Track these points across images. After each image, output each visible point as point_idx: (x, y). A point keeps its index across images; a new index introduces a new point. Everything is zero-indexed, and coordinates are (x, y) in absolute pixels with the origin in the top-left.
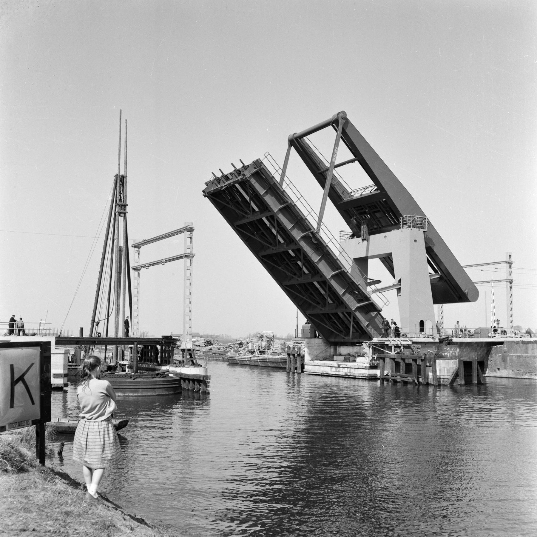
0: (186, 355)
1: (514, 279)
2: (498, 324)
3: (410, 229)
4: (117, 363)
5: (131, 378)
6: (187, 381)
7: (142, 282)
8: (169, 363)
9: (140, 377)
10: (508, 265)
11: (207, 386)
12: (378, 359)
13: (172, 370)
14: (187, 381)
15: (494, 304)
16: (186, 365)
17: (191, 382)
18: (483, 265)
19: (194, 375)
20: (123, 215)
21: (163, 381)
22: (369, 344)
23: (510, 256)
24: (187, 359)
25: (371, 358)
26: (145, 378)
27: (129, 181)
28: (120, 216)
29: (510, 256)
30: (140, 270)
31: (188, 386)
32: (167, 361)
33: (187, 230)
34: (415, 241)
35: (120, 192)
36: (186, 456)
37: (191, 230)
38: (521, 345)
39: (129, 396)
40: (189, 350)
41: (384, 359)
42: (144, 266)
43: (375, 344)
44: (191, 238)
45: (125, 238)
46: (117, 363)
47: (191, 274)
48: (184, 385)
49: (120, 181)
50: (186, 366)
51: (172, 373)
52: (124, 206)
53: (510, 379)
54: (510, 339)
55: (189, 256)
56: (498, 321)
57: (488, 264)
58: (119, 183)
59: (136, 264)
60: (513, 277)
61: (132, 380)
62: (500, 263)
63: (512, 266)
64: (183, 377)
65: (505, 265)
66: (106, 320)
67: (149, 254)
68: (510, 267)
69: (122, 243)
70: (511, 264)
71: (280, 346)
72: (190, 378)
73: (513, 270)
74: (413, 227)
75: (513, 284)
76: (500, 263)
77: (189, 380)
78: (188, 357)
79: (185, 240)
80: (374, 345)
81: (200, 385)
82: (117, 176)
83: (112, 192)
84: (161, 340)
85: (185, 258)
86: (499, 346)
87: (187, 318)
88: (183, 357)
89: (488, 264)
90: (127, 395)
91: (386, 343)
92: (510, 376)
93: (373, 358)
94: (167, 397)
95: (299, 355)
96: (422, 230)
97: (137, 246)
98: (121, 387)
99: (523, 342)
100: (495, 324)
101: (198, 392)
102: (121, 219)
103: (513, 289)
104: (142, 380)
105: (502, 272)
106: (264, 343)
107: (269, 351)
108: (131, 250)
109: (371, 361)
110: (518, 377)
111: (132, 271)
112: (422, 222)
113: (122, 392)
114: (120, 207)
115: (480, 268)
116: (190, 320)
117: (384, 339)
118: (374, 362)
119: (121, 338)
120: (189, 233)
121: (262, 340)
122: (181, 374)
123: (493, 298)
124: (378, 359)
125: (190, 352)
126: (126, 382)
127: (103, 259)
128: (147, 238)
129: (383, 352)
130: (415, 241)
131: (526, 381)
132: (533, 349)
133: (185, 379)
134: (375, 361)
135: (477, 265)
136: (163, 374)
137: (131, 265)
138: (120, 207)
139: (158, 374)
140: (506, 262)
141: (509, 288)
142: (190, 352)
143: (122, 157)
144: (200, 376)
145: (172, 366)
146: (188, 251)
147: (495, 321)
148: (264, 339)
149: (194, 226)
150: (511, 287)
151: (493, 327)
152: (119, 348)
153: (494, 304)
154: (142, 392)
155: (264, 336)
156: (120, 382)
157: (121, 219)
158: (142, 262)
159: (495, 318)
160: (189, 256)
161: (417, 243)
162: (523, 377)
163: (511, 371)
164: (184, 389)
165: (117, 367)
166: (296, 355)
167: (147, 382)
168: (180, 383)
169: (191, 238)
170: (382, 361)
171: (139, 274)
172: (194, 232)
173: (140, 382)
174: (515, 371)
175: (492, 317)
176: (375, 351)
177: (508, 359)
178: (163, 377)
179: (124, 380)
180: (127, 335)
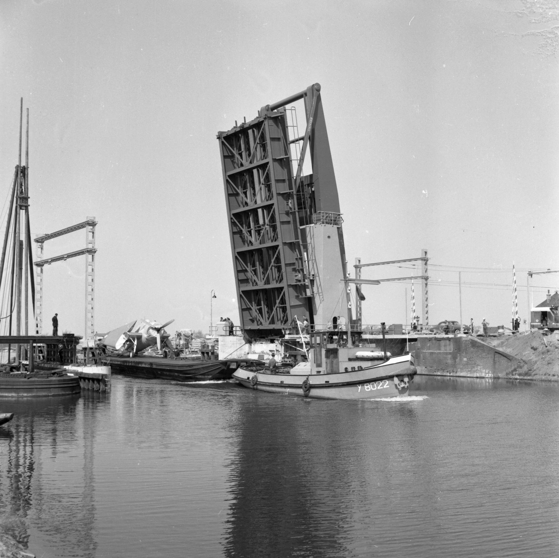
0: (88, 354)
1: (429, 275)
2: (418, 321)
3: (323, 225)
4: (20, 363)
5: (25, 377)
6: (87, 381)
7: (47, 278)
8: (72, 362)
9: (35, 376)
10: (424, 262)
11: (106, 386)
12: (290, 356)
13: (71, 370)
14: (87, 381)
15: (414, 301)
16: (88, 364)
17: (91, 381)
18: (399, 262)
19: (94, 374)
20: (24, 208)
21: (59, 381)
22: (281, 342)
23: (426, 253)
24: (89, 358)
25: (283, 356)
26: (40, 377)
27: (31, 173)
28: (21, 209)
29: (426, 253)
30: (43, 265)
31: (88, 385)
32: (72, 360)
33: (89, 224)
34: (329, 237)
35: (21, 185)
36: (89, 457)
37: (93, 224)
38: (434, 341)
39: (23, 397)
40: (91, 349)
41: (295, 356)
42: (46, 262)
43: (287, 342)
44: (93, 233)
45: (27, 232)
46: (20, 363)
47: (93, 269)
48: (82, 384)
49: (21, 172)
50: (88, 365)
51: (71, 373)
52: (26, 199)
53: (423, 376)
54: (425, 336)
55: (92, 252)
56: (418, 317)
57: (405, 261)
58: (20, 175)
59: (39, 260)
60: (429, 274)
61: (26, 380)
62: (416, 260)
63: (428, 262)
64: (83, 376)
65: (420, 262)
66: (9, 318)
67: (52, 248)
68: (426, 264)
69: (23, 237)
70: (427, 260)
71: (199, 345)
72: (90, 377)
73: (429, 267)
74: (327, 223)
75: (428, 281)
76: (416, 260)
77: (89, 379)
78: (91, 355)
79: (87, 235)
80: (286, 342)
81: (99, 384)
82: (17, 167)
83: (13, 184)
84: (62, 339)
85: (87, 254)
86: (412, 343)
87: (89, 315)
88: (85, 356)
89: (405, 261)
90: (21, 395)
91: (298, 340)
92: (423, 373)
93: (285, 356)
94: (63, 397)
95: (213, 353)
96: (336, 226)
97: (41, 241)
98: (15, 387)
99: (436, 339)
100: (415, 321)
101: (98, 391)
102: (23, 212)
103: (428, 286)
104: (36, 379)
105: (418, 269)
106: (182, 342)
107: (187, 350)
108: (34, 245)
109: (283, 358)
110: (431, 374)
111: (34, 267)
112: (336, 218)
113: (15, 392)
114: (21, 200)
115: (399, 264)
116: (92, 317)
117: (295, 336)
118: (286, 359)
119: (23, 337)
120: (91, 227)
121: (180, 339)
122: (82, 373)
123: (413, 294)
124: (290, 356)
125: (92, 351)
126: (19, 382)
127: (4, 254)
128: (50, 232)
129: (296, 350)
130: (329, 237)
131: (439, 378)
132: (445, 346)
133: (85, 379)
134: (288, 358)
135: (393, 262)
136: (60, 374)
137: (34, 260)
138: (21, 200)
139: (54, 374)
140: (422, 259)
141: (425, 285)
142: (92, 351)
143: (23, 147)
144: (99, 374)
145: (74, 366)
146: (90, 246)
147: (415, 318)
148: (182, 337)
149: (96, 220)
150: (426, 284)
151: (515, 319)
152: (22, 348)
153: (414, 301)
154: (37, 392)
155: (182, 334)
156: (14, 382)
157: (23, 212)
158: (45, 257)
159: (415, 315)
160: (92, 252)
161: (330, 240)
162: (435, 374)
163: (424, 368)
164: (84, 389)
165: (20, 367)
166: (210, 353)
167: (42, 382)
168: (78, 383)
169: (93, 233)
170: (293, 358)
171: (42, 270)
172: (96, 227)
173: (34, 381)
174: (428, 367)
175: (412, 314)
176: (287, 348)
177: (422, 355)
178: (60, 376)
179: (17, 379)
180: (19, 334)
